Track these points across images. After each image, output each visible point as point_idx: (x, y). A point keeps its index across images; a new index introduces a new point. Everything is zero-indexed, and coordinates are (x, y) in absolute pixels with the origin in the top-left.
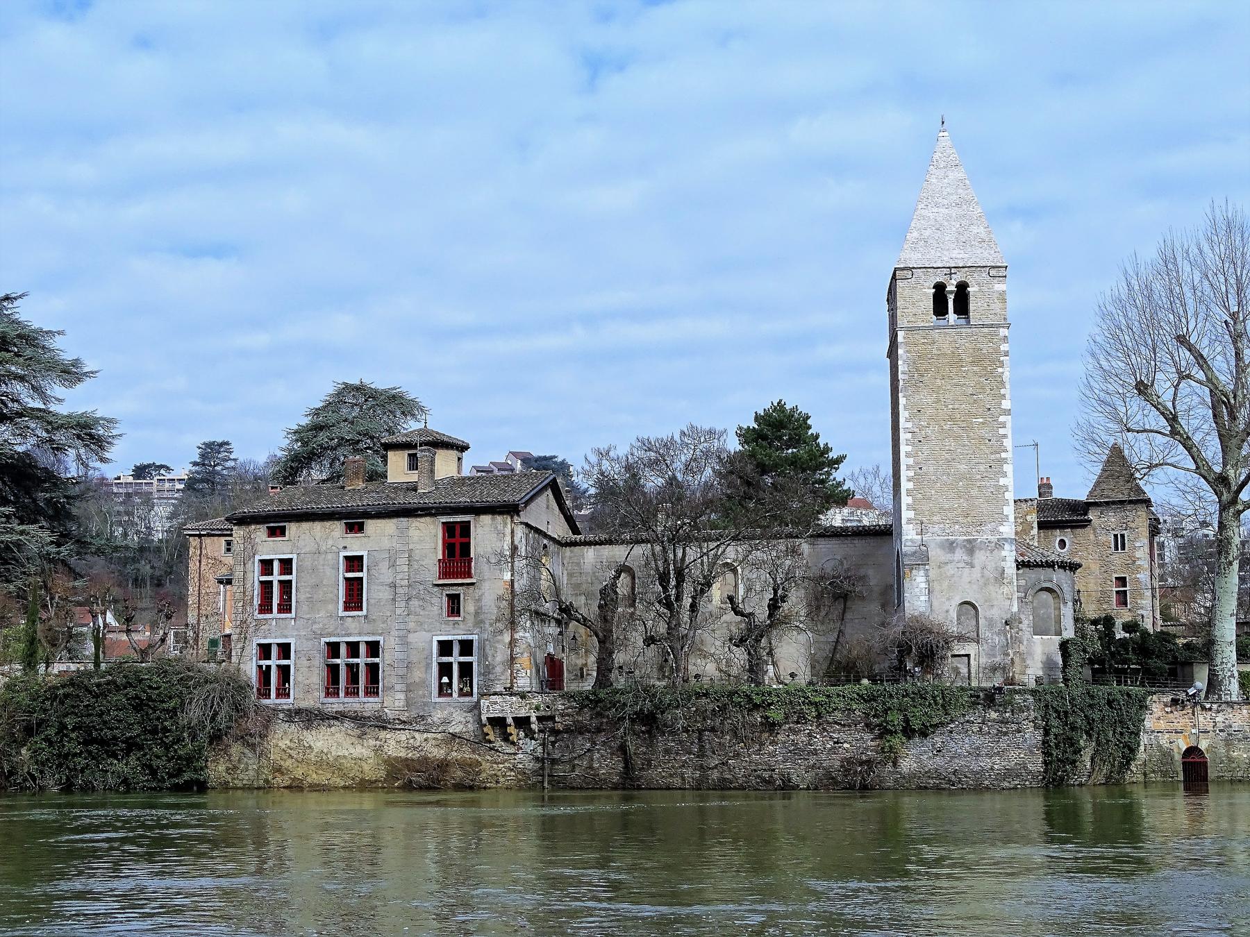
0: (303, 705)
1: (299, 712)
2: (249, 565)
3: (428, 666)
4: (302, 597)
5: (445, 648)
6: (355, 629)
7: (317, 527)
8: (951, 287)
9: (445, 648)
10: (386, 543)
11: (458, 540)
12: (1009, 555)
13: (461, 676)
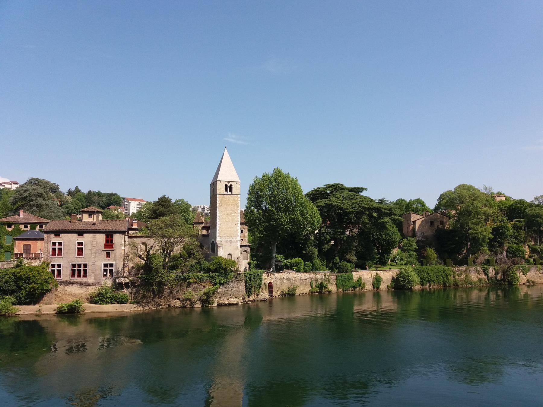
0: (65, 280)
1: (63, 282)
2: (49, 244)
3: (101, 270)
4: (65, 252)
5: (105, 265)
6: (80, 260)
7: (70, 235)
8: (229, 186)
9: (105, 265)
10: (90, 239)
11: (110, 239)
12: (239, 244)
13: (110, 272)
